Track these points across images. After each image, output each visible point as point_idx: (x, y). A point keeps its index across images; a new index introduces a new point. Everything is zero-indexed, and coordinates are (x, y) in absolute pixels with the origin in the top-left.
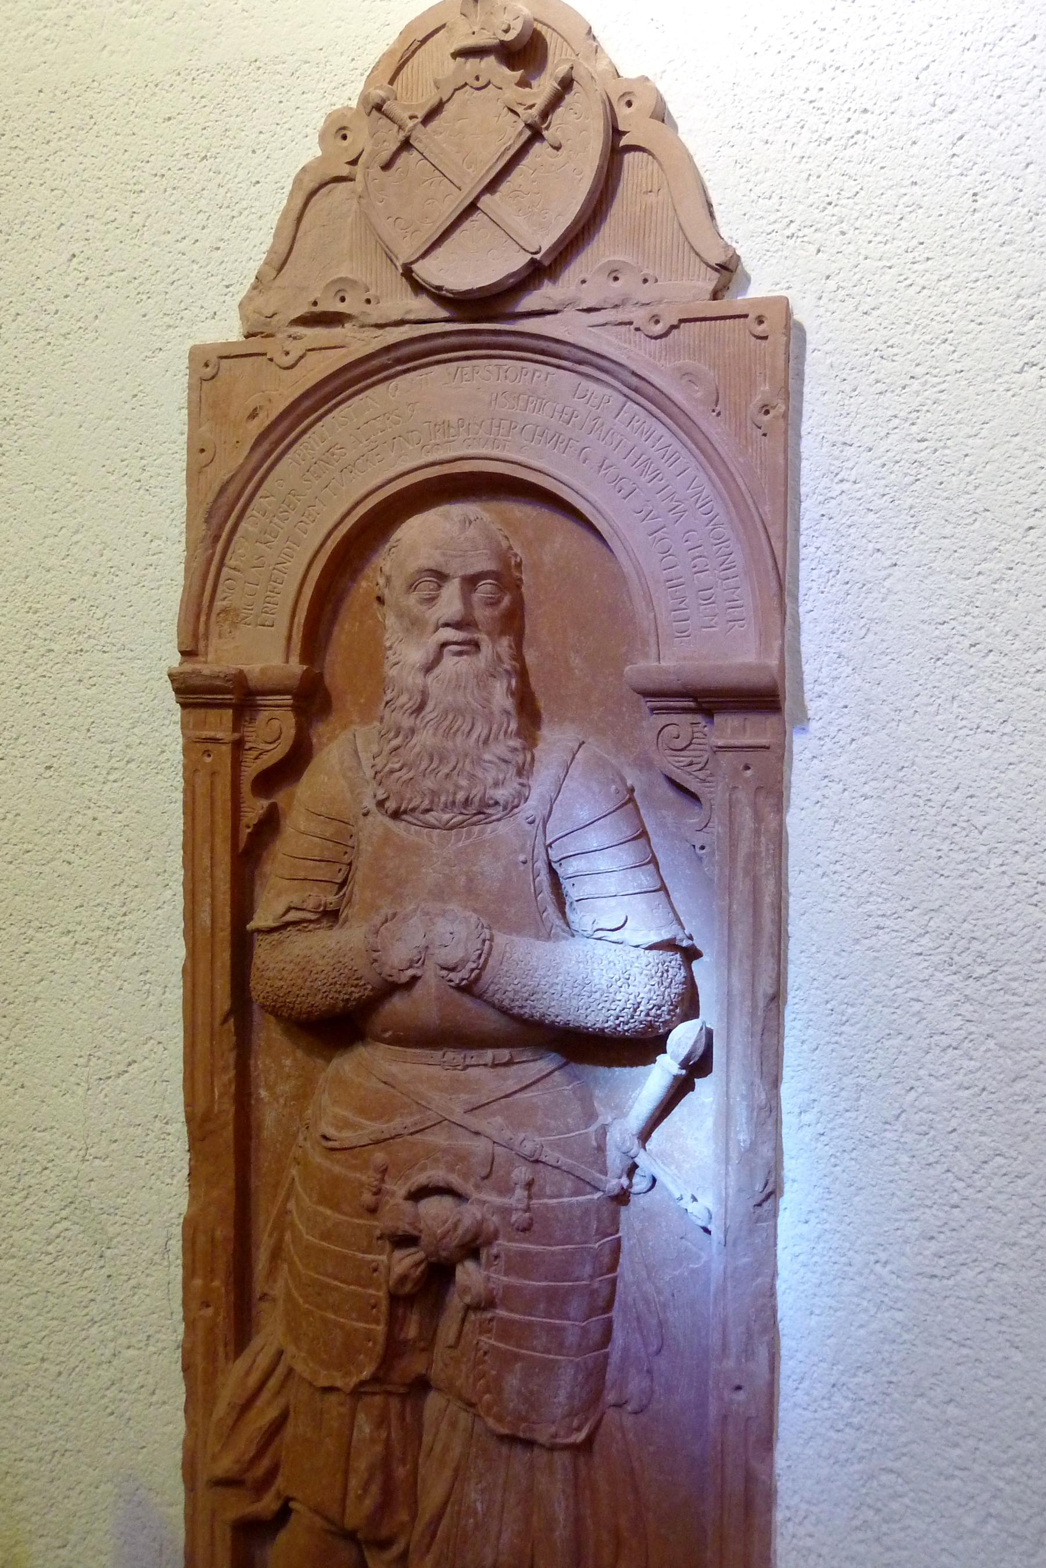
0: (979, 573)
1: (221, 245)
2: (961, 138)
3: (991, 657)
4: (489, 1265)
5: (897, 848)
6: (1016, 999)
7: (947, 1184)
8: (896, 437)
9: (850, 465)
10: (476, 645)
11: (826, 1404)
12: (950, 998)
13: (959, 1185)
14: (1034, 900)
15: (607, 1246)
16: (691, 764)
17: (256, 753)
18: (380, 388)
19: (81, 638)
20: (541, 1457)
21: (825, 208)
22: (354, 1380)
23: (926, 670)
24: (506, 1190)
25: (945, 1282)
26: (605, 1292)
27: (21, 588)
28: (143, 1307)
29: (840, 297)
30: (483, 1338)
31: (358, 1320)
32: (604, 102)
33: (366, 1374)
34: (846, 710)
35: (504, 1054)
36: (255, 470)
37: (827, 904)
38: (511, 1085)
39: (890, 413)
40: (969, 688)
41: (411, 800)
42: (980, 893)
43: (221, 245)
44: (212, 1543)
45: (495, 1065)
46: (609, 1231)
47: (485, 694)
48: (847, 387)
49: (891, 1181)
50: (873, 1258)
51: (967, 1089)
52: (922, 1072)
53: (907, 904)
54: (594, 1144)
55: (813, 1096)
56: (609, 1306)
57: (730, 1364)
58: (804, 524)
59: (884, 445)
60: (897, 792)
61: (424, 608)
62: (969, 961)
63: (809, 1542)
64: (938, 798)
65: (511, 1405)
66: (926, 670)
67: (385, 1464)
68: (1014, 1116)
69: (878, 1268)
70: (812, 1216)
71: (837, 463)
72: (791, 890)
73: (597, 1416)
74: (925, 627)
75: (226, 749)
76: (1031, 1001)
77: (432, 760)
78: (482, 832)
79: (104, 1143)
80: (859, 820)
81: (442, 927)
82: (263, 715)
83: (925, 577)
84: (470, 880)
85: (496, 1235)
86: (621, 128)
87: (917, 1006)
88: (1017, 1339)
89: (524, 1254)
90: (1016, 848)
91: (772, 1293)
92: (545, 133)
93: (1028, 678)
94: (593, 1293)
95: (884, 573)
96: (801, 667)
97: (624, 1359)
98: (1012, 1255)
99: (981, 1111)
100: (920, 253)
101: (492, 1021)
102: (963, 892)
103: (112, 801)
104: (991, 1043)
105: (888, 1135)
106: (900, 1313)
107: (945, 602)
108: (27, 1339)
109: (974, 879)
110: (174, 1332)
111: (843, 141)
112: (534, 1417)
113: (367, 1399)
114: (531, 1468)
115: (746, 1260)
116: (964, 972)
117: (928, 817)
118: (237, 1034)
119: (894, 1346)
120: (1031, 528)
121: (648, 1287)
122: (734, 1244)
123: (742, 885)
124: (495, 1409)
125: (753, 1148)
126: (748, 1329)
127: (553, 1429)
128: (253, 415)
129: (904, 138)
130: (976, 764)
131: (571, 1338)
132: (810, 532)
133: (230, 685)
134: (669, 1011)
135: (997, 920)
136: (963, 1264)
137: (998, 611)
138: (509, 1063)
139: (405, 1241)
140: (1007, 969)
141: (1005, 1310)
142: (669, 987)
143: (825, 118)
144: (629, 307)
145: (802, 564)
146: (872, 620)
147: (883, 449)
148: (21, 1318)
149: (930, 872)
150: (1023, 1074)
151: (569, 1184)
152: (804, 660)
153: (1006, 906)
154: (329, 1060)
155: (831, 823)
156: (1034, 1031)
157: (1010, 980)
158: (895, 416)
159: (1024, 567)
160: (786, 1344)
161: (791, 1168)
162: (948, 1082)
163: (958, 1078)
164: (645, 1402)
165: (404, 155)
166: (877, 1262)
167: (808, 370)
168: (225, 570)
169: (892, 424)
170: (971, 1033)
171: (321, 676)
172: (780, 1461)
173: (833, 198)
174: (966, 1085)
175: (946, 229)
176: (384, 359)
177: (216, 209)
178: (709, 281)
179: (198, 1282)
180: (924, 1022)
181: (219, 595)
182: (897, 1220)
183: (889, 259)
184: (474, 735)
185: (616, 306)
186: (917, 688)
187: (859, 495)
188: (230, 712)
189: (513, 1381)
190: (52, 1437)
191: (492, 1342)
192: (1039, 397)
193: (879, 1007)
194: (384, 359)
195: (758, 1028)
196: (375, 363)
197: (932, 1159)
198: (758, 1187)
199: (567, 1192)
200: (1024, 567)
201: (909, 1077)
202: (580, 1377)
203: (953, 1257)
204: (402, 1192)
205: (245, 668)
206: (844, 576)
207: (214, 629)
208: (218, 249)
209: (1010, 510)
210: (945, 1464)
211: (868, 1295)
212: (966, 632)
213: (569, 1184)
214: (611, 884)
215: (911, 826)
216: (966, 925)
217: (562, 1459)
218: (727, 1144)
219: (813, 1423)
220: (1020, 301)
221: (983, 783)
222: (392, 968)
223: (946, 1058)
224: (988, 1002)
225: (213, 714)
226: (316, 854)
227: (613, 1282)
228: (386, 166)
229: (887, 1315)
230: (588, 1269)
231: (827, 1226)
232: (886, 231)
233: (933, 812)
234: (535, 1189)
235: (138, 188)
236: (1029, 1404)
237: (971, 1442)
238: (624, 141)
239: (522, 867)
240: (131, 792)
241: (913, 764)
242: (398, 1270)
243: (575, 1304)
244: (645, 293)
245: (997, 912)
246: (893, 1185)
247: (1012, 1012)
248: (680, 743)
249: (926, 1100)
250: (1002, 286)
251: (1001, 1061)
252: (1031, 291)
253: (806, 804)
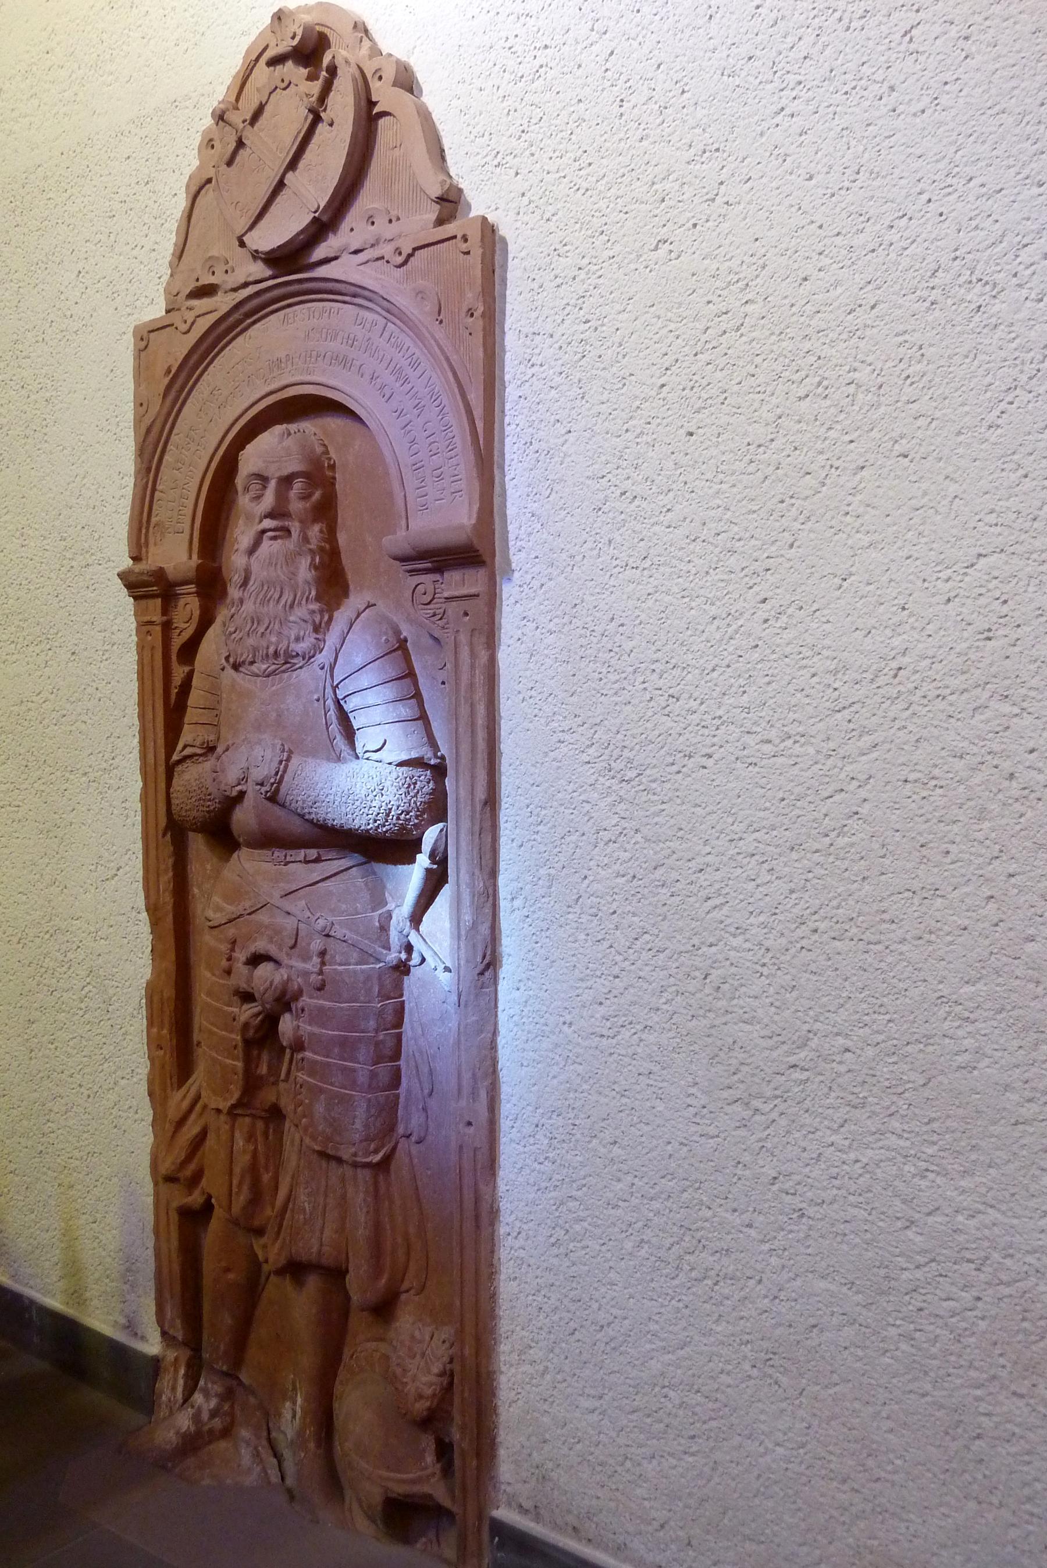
0: (627, 431)
2: (612, 53)
3: (637, 502)
4: (298, 1017)
5: (571, 673)
6: (656, 798)
7: (611, 957)
8: (569, 322)
9: (537, 351)
10: (287, 531)
11: (532, 1140)
12: (609, 800)
13: (619, 958)
14: (666, 711)
15: (390, 1007)
16: (434, 615)
18: (240, 340)
19: (87, 556)
21: (520, 137)
23: (591, 520)
24: (306, 958)
25: (610, 1040)
26: (390, 1043)
27: (57, 523)
28: (129, 1048)
29: (531, 210)
30: (299, 1074)
31: (227, 1058)
32: (355, 80)
34: (537, 560)
35: (313, 853)
36: (169, 414)
37: (526, 724)
39: (565, 302)
40: (620, 532)
41: (242, 655)
42: (629, 708)
43: (156, 247)
44: (168, 1225)
45: (307, 862)
46: (392, 995)
47: (292, 569)
48: (535, 285)
49: (573, 955)
50: (562, 1019)
51: (623, 876)
52: (592, 863)
53: (579, 720)
54: (377, 924)
55: (520, 885)
56: (397, 1055)
57: (463, 1103)
58: (508, 406)
59: (561, 330)
60: (572, 626)
61: (253, 504)
62: (622, 766)
63: (522, 1253)
64: (599, 629)
65: (320, 1128)
66: (591, 520)
67: (253, 1169)
68: (656, 899)
69: (565, 1028)
70: (521, 984)
71: (529, 351)
72: (502, 714)
73: (392, 1144)
74: (589, 482)
75: (158, 628)
76: (666, 799)
77: (253, 623)
78: (290, 677)
79: (105, 927)
80: (546, 652)
81: (258, 751)
82: (182, 602)
83: (590, 439)
84: (279, 716)
85: (300, 993)
86: (374, 100)
87: (587, 807)
88: (660, 1092)
89: (321, 1009)
90: (653, 667)
91: (493, 1047)
92: (322, 115)
93: (662, 518)
94: (377, 1044)
95: (562, 440)
96: (506, 527)
97: (407, 1100)
98: (656, 1019)
99: (633, 895)
100: (585, 160)
101: (296, 827)
102: (617, 707)
103: (105, 674)
104: (638, 837)
105: (570, 916)
106: (581, 1067)
107: (603, 458)
108: (73, 1071)
109: (625, 696)
110: (143, 1068)
111: (531, 77)
112: (338, 1139)
113: (240, 1120)
114: (343, 1180)
115: (474, 1018)
116: (619, 776)
117: (592, 645)
118: (173, 843)
119: (577, 1095)
120: (663, 386)
121: (422, 1042)
122: (466, 1005)
123: (464, 711)
124: (310, 1130)
125: (474, 925)
126: (474, 1075)
129: (572, 64)
130: (625, 597)
131: (362, 1078)
132: (512, 412)
133: (151, 579)
134: (417, 817)
135: (640, 730)
136: (622, 1026)
137: (640, 461)
138: (317, 860)
140: (648, 772)
141: (652, 1067)
142: (416, 796)
143: (519, 60)
144: (381, 245)
145: (507, 440)
146: (554, 480)
147: (560, 334)
148: (69, 1055)
149: (594, 692)
150: (662, 862)
151: (355, 955)
152: (509, 521)
153: (646, 718)
155: (528, 656)
156: (668, 825)
157: (651, 781)
158: (568, 304)
159: (659, 421)
160: (505, 1090)
161: (508, 944)
162: (610, 871)
163: (616, 867)
164: (422, 1134)
165: (241, 152)
166: (564, 1023)
167: (509, 275)
168: (157, 494)
169: (566, 312)
170: (625, 829)
171: (220, 569)
172: (502, 1187)
173: (525, 127)
174: (622, 873)
175: (601, 136)
176: (236, 316)
177: (153, 220)
178: (432, 213)
179: (155, 1030)
180: (592, 821)
181: (154, 513)
182: (577, 988)
183: (564, 169)
184: (283, 602)
185: (373, 246)
186: (585, 536)
187: (544, 376)
188: (159, 601)
189: (320, 1108)
190: (87, 1142)
191: (305, 1077)
192: (668, 269)
193: (562, 809)
194: (236, 316)
195: (477, 828)
196: (231, 319)
197: (600, 937)
198: (479, 959)
199: (353, 961)
200: (659, 421)
201: (583, 867)
202: (373, 1111)
203: (616, 1019)
205: (164, 566)
206: (536, 446)
207: (151, 540)
209: (648, 371)
210: (611, 1195)
211: (559, 1050)
212: (618, 483)
213: (355, 956)
214: (377, 714)
215: (581, 654)
216: (619, 736)
217: (364, 1175)
218: (459, 923)
219: (523, 1156)
220: (655, 187)
221: (630, 612)
222: (226, 785)
223: (609, 850)
224: (636, 801)
227: (399, 1037)
228: (230, 163)
229: (572, 1067)
230: (372, 1024)
231: (531, 993)
232: (561, 146)
233: (595, 640)
234: (327, 957)
236: (669, 1147)
237: (629, 1178)
238: (376, 110)
239: (316, 704)
240: (115, 667)
241: (582, 602)
242: (243, 1018)
243: (363, 1051)
244: (390, 231)
245: (640, 723)
246: (574, 959)
247: (653, 809)
248: (427, 598)
249: (596, 886)
250: (640, 177)
251: (645, 851)
252: (662, 176)
253: (511, 642)
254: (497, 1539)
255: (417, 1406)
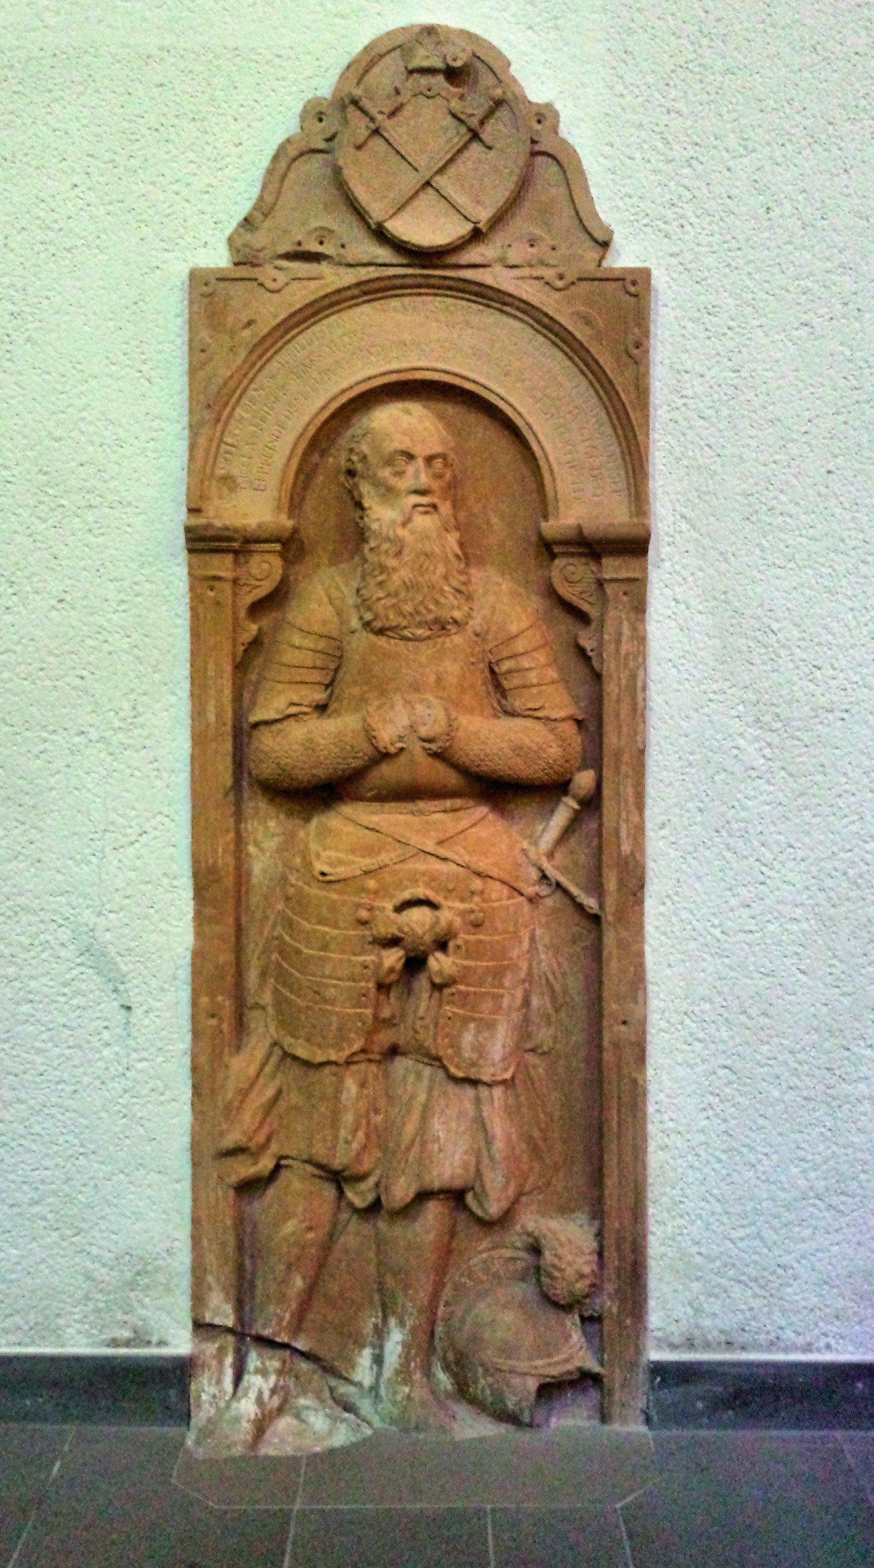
1: (210, 189)
10: (435, 507)
17: (248, 589)
20: (484, 1092)
22: (347, 1052)
33: (356, 1047)
35: (458, 802)
38: (464, 824)
43: (210, 189)
78: (443, 643)
114: (478, 1101)
127: (492, 1070)
128: (250, 323)
139: (393, 942)
154: (308, 820)
168: (223, 446)
204: (389, 906)
208: (207, 192)
225: (216, 559)
226: (309, 663)
235: (133, 137)
247: (797, 752)
254: (659, 1379)
255: (578, 1285)
